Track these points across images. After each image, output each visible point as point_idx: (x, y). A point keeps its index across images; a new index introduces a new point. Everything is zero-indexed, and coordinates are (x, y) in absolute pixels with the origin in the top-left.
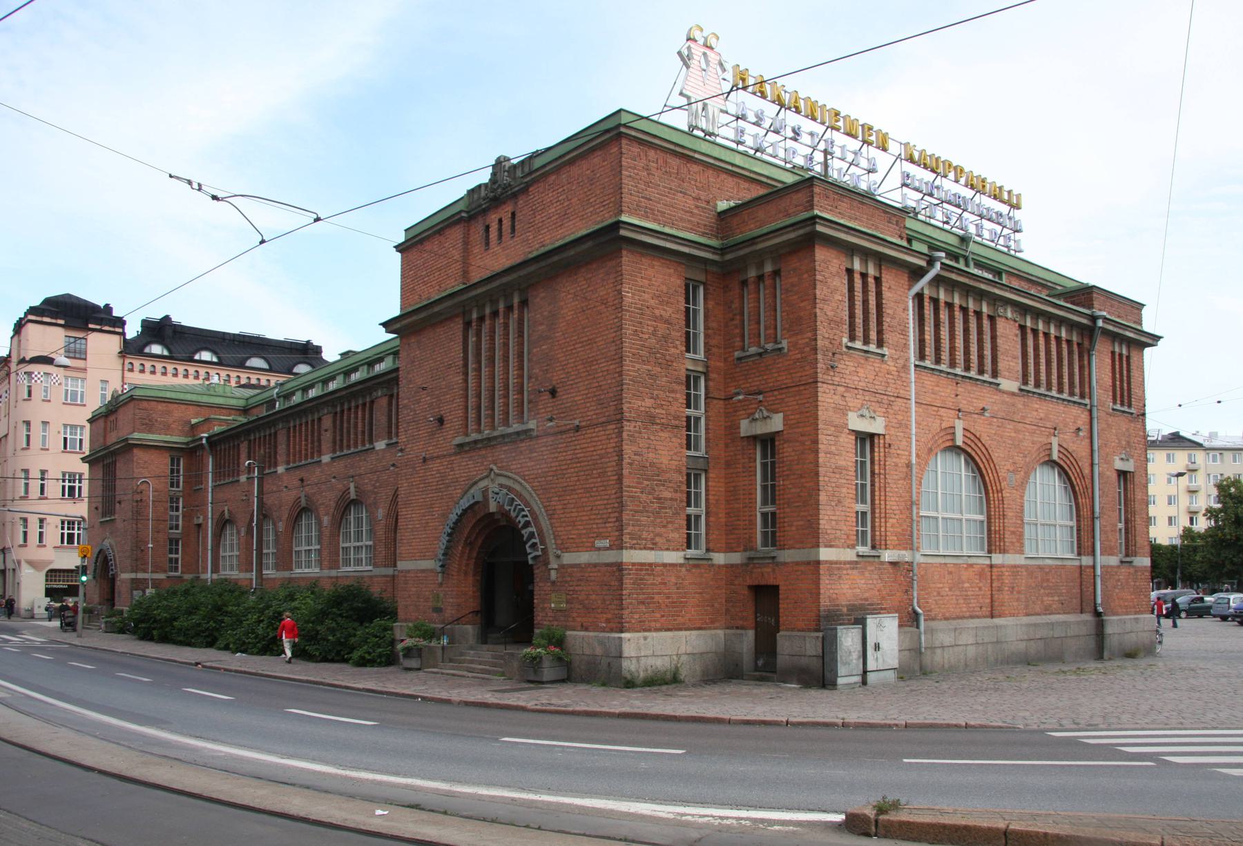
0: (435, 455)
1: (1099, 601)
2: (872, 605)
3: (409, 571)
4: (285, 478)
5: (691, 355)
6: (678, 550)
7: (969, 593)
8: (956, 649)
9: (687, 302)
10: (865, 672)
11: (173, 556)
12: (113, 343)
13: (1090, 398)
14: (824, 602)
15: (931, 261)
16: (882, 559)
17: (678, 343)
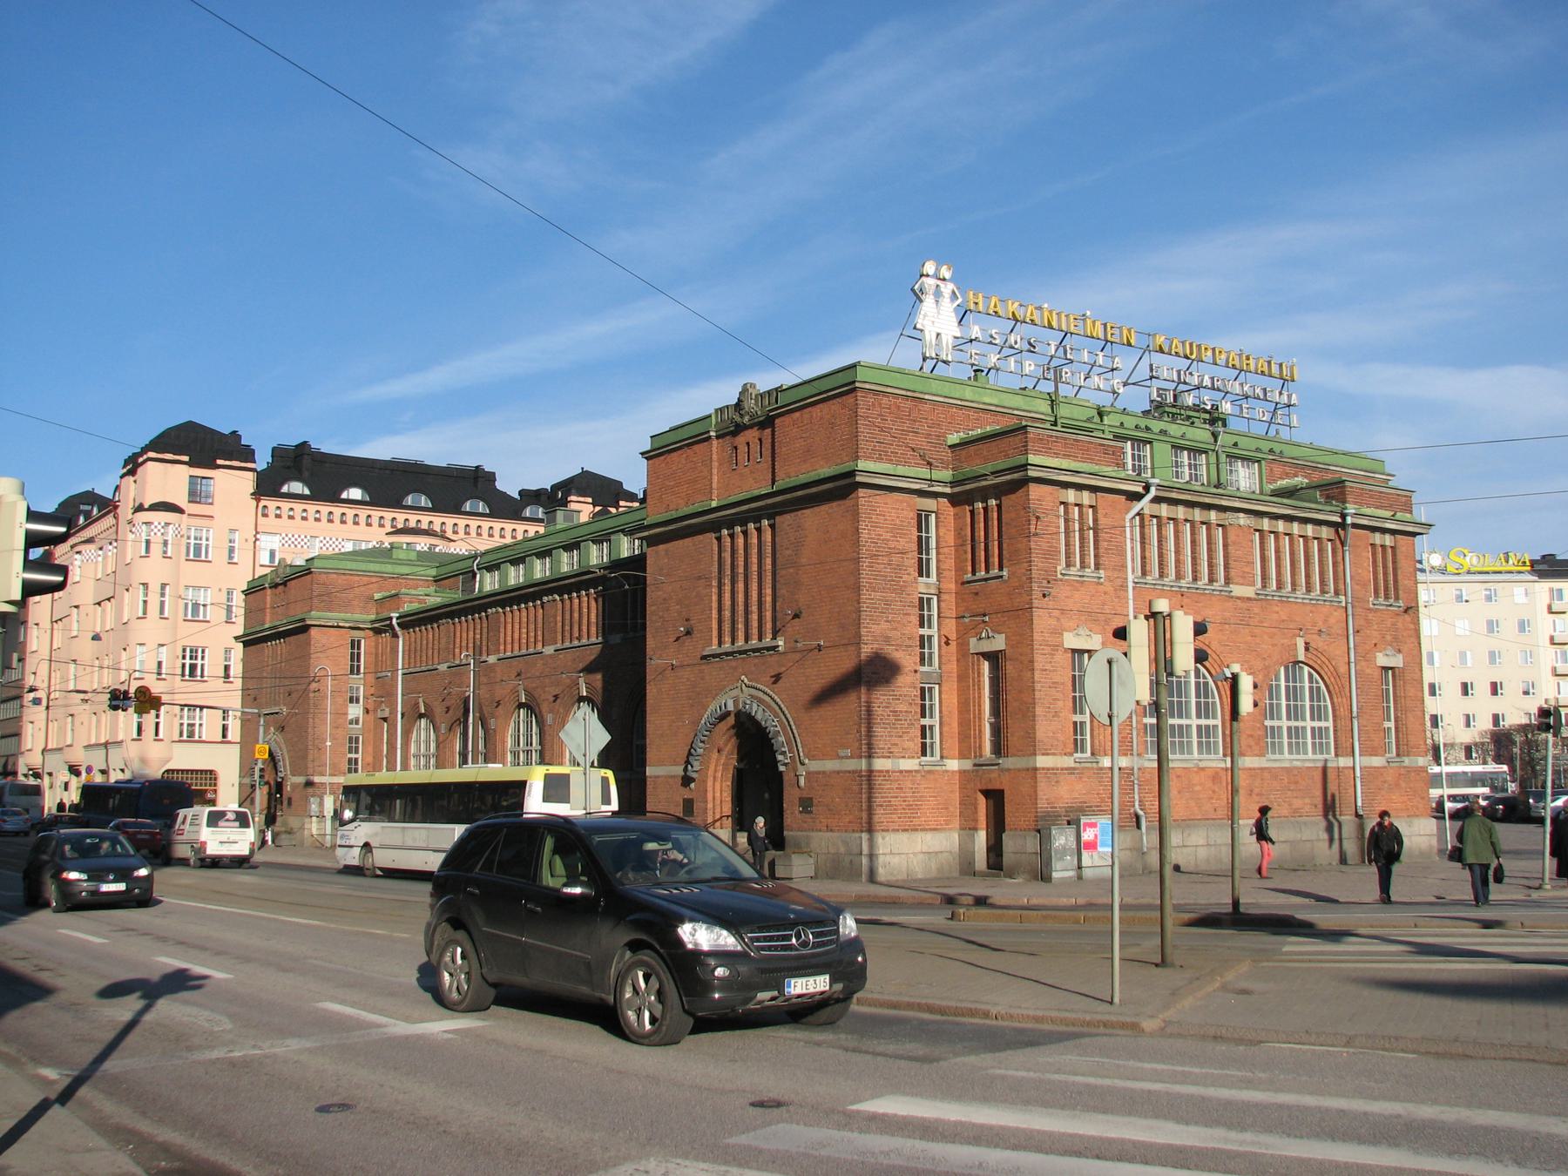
0: (685, 663)
1: (1359, 804)
2: (1091, 807)
3: (658, 777)
4: (498, 669)
5: (924, 579)
6: (913, 757)
7: (1201, 796)
8: (1185, 850)
9: (920, 530)
10: (1080, 867)
11: (353, 756)
12: (247, 481)
13: (1345, 595)
14: (1042, 805)
15: (1147, 488)
16: (1100, 765)
17: (912, 569)
